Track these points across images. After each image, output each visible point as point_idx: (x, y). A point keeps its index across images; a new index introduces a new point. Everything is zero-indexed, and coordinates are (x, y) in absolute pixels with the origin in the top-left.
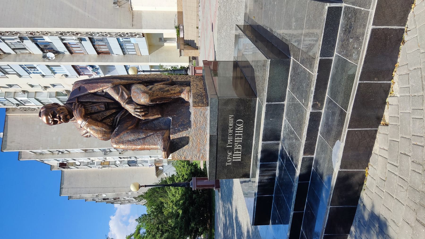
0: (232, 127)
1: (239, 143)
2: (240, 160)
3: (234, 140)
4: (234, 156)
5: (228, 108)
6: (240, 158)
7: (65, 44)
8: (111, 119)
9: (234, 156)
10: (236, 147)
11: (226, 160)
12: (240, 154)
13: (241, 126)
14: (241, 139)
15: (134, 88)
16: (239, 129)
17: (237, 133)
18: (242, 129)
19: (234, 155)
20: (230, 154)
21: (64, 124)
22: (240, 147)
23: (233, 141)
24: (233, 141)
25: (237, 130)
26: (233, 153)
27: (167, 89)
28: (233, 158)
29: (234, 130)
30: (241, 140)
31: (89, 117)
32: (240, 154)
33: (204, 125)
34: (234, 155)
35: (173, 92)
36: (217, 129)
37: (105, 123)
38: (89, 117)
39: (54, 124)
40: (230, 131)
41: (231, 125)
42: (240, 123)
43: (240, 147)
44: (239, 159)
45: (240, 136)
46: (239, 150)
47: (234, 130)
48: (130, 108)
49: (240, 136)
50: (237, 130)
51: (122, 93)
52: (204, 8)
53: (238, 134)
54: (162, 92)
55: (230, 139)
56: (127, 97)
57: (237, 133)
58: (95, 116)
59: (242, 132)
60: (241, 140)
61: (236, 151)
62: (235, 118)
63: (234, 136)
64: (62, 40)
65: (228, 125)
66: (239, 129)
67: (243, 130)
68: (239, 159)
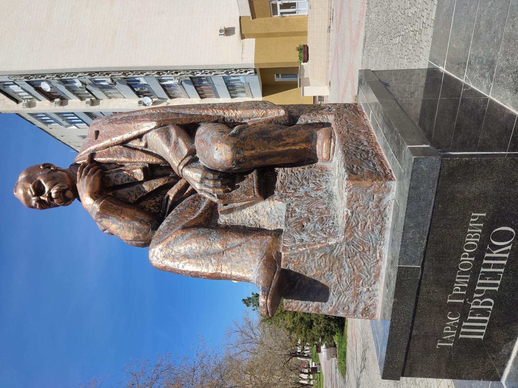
0: (473, 246)
1: (489, 294)
2: (482, 337)
3: (472, 284)
4: (465, 327)
5: (474, 189)
6: (484, 331)
7: (163, 86)
8: (158, 199)
9: (465, 327)
10: (477, 303)
11: (439, 336)
12: (484, 321)
13: (507, 245)
14: (499, 282)
15: (200, 130)
16: (495, 254)
17: (488, 266)
18: (507, 255)
19: (464, 324)
20: (455, 319)
21: (62, 208)
22: (489, 304)
23: (471, 289)
24: (471, 289)
25: (488, 258)
26: (464, 318)
27: (277, 132)
28: (462, 330)
29: (479, 256)
30: (495, 285)
31: (111, 194)
32: (484, 321)
33: (377, 232)
34: (464, 324)
35: (291, 140)
36: (425, 253)
37: (142, 209)
38: (111, 194)
39: (42, 208)
40: (466, 259)
41: (472, 241)
42: (503, 236)
43: (489, 304)
44: (481, 334)
45: (494, 276)
46: (483, 312)
47: (479, 256)
48: (193, 176)
49: (494, 276)
50: (488, 258)
51: (176, 143)
52: (340, 22)
53: (491, 270)
54: (264, 139)
55: (460, 283)
56: (185, 151)
57: (488, 266)
58: (123, 192)
59: (504, 262)
60: (495, 285)
61: (473, 314)
62: (489, 226)
63: (475, 273)
64: (160, 81)
65: (462, 242)
66: (495, 254)
67: (509, 259)
68: (481, 334)
